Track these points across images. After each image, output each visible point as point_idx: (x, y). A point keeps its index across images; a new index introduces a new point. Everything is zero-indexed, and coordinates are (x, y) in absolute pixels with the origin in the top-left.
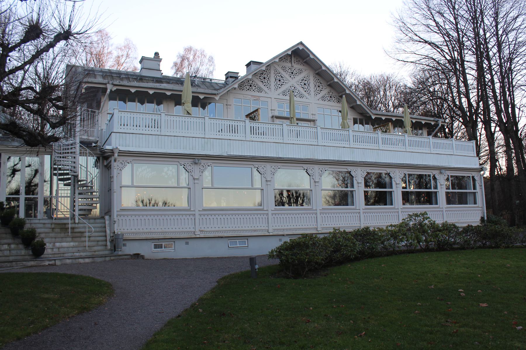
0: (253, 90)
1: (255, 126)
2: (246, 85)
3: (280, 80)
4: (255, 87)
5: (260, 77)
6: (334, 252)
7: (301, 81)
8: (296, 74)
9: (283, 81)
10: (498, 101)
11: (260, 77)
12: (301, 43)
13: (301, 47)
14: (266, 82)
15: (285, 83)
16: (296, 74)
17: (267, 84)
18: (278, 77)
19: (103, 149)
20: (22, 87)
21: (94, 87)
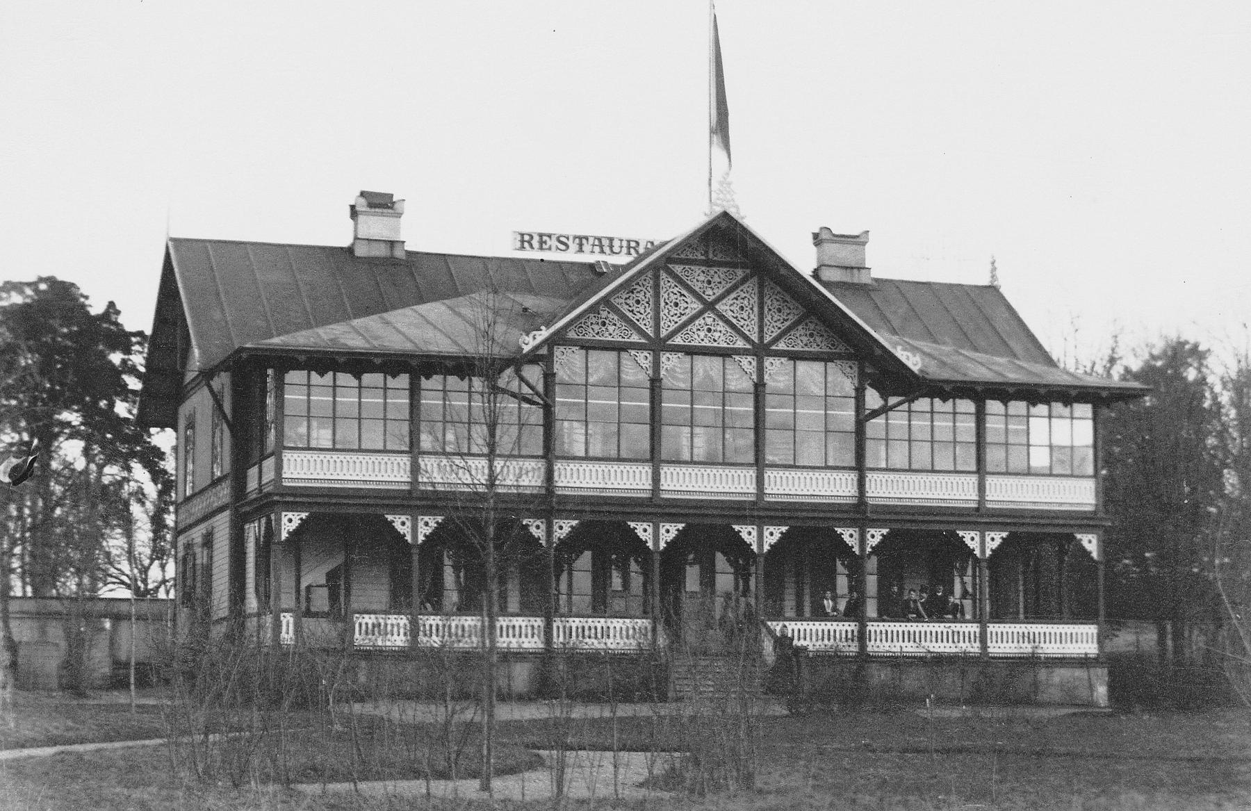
0: (611, 334)
1: (1074, 632)
2: (592, 324)
3: (676, 305)
4: (615, 325)
5: (626, 299)
6: (147, 514)
7: (732, 302)
8: (720, 283)
9: (686, 305)
10: (70, 331)
11: (626, 299)
12: (725, 215)
13: (724, 225)
14: (642, 311)
15: (729, 304)
16: (720, 283)
17: (642, 317)
18: (673, 297)
19: (496, 609)
20: (765, 342)
21: (188, 335)
